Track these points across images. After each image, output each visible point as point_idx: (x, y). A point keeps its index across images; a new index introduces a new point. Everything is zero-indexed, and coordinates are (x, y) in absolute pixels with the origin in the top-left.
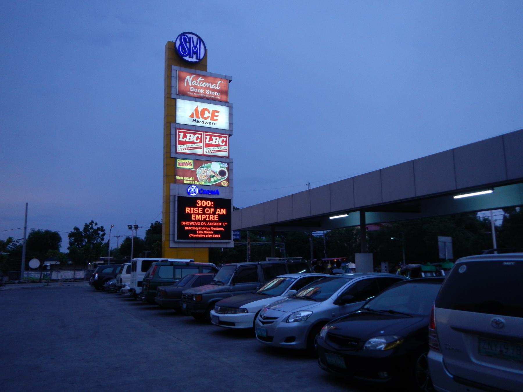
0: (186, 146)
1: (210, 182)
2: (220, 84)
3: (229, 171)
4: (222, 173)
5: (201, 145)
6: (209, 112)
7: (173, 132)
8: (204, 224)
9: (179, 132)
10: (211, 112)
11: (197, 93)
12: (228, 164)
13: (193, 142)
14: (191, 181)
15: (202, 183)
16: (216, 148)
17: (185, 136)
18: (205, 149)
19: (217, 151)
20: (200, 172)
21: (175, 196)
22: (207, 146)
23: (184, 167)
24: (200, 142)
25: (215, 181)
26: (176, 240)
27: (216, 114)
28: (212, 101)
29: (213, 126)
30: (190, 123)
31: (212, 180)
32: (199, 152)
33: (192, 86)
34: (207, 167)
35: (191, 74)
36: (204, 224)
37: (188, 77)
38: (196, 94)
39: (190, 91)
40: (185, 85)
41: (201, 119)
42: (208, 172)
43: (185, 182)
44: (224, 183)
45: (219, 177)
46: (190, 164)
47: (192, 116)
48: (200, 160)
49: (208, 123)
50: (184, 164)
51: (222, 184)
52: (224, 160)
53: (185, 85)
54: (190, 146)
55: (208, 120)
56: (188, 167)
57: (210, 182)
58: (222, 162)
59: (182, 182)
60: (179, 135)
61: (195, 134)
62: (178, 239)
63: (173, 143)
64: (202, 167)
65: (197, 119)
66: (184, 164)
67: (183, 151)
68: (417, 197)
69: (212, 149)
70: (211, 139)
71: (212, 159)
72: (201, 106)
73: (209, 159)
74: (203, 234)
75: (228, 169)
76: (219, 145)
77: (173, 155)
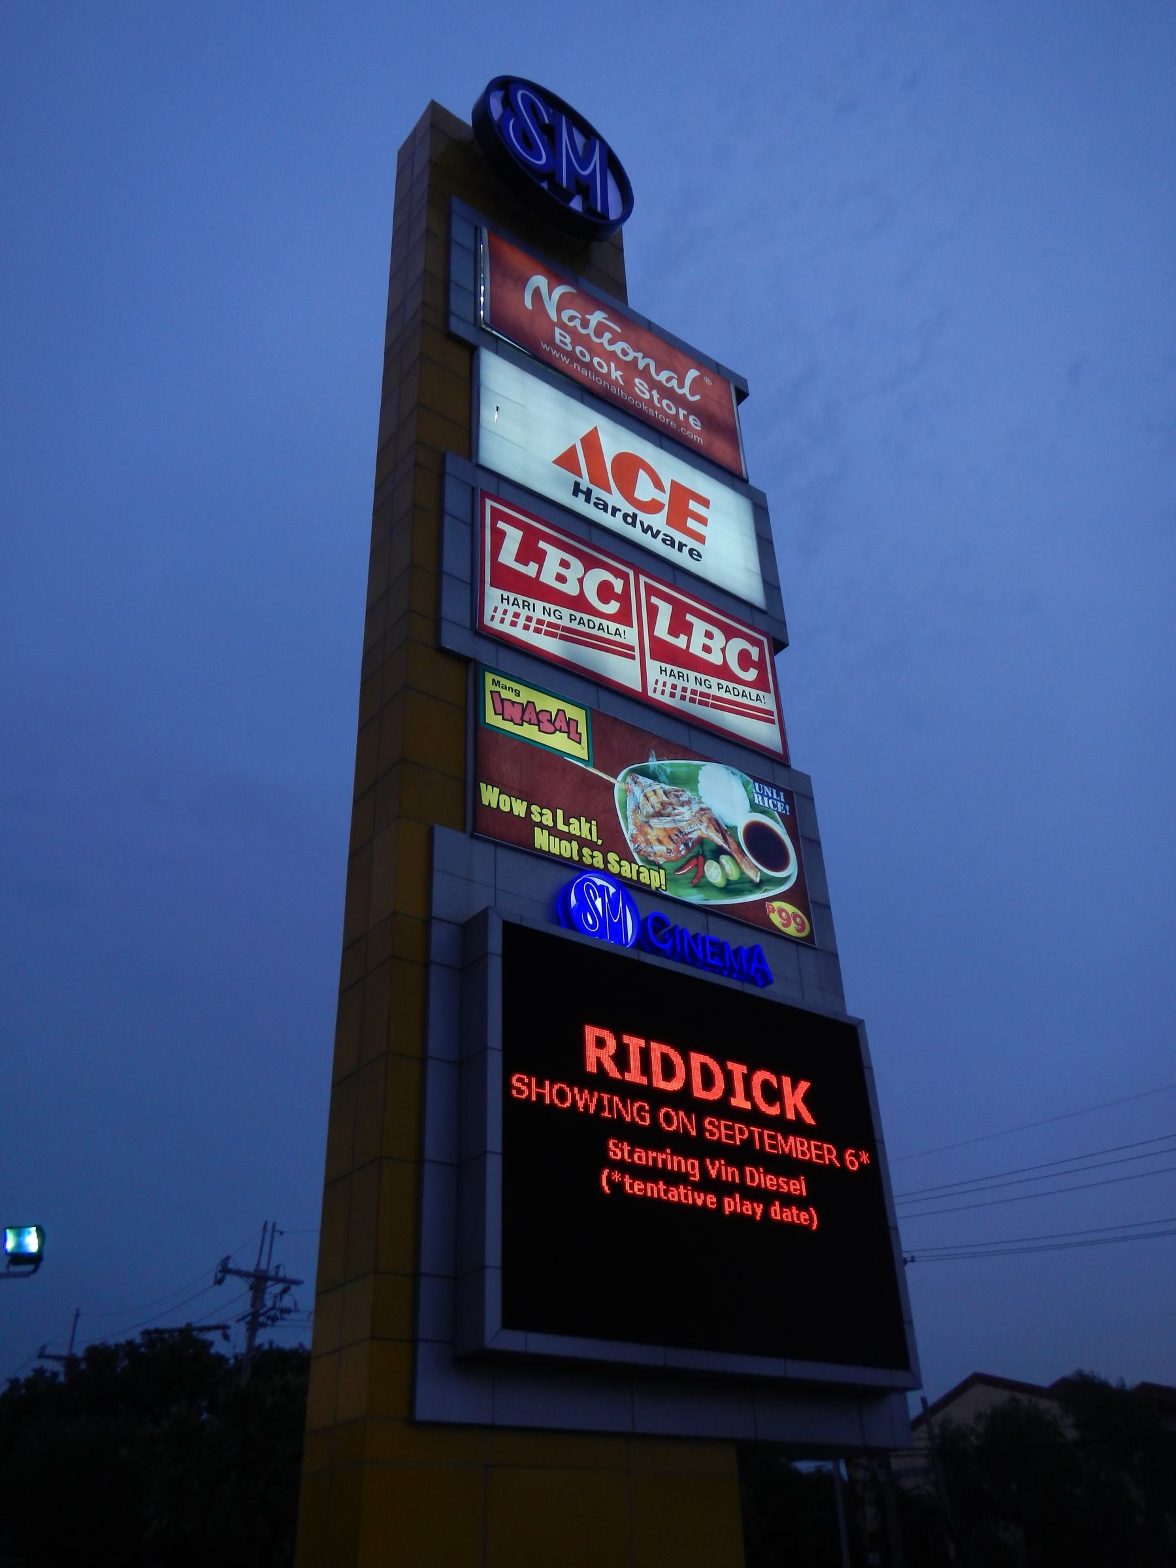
0: (539, 609)
1: (699, 882)
2: (694, 380)
3: (791, 833)
4: (761, 842)
5: (630, 636)
6: (658, 485)
7: (455, 501)
8: (679, 1121)
9: (497, 515)
10: (667, 486)
11: (589, 366)
12: (789, 799)
13: (579, 603)
14: (583, 842)
15: (656, 879)
16: (714, 686)
17: (530, 552)
18: (653, 666)
19: (720, 704)
20: (632, 794)
21: (472, 930)
22: (663, 652)
23: (529, 732)
24: (623, 617)
25: (730, 888)
26: (498, 1336)
27: (693, 506)
28: (664, 441)
29: (682, 559)
30: (554, 486)
31: (714, 872)
32: (624, 672)
33: (563, 326)
34: (673, 779)
35: (556, 279)
36: (679, 1121)
37: (539, 281)
38: (584, 372)
39: (551, 342)
40: (528, 303)
41: (615, 498)
42: (686, 813)
43: (542, 840)
44: (784, 917)
45: (754, 870)
46: (569, 728)
47: (567, 461)
48: (637, 729)
49: (654, 532)
50: (527, 713)
51: (775, 918)
52: (764, 768)
53: (528, 303)
54: (565, 617)
55: (658, 521)
56: (558, 741)
57: (699, 882)
58: (756, 779)
59: (515, 837)
60: (498, 537)
61: (590, 564)
62: (510, 1321)
63: (454, 560)
64: (645, 773)
65: (597, 492)
66: (527, 713)
67: (518, 633)
68: (894, 1209)
69: (692, 680)
70: (679, 626)
71: (699, 742)
72: (616, 440)
73: (679, 735)
74: (706, 1184)
75: (790, 822)
76: (723, 672)
77: (455, 639)
